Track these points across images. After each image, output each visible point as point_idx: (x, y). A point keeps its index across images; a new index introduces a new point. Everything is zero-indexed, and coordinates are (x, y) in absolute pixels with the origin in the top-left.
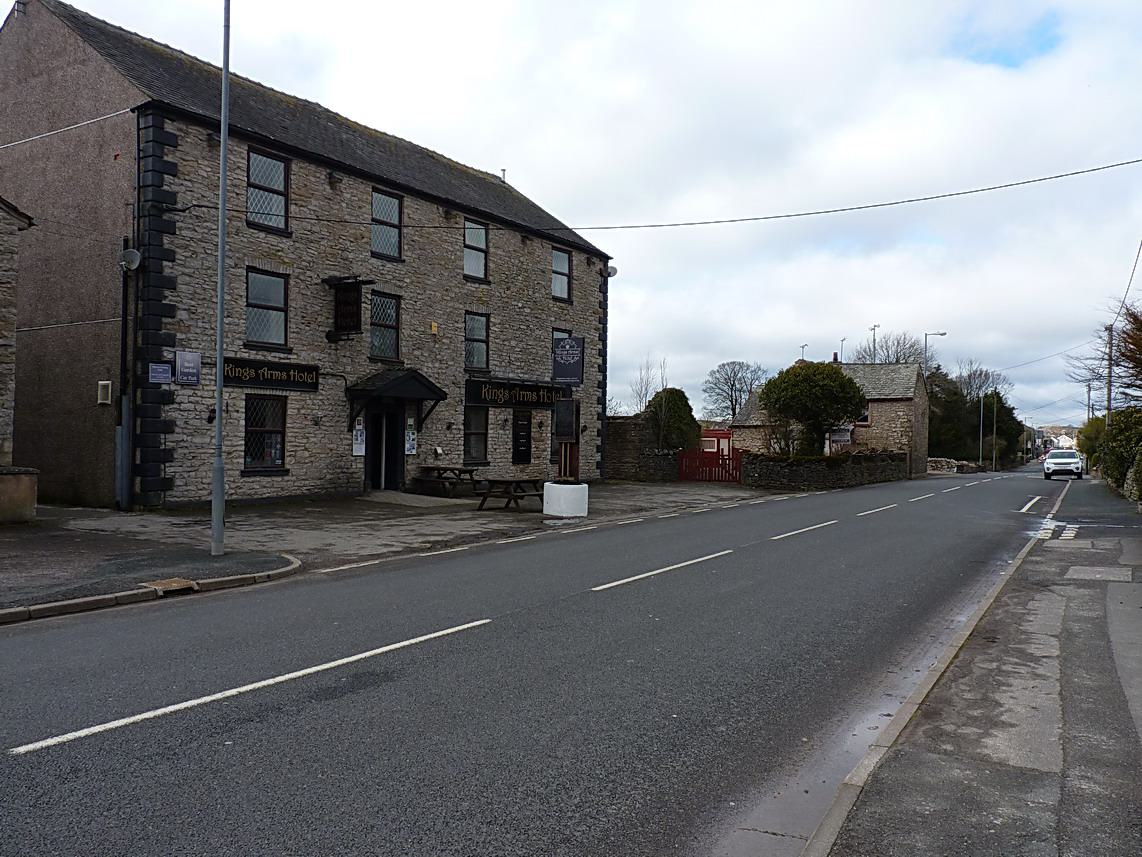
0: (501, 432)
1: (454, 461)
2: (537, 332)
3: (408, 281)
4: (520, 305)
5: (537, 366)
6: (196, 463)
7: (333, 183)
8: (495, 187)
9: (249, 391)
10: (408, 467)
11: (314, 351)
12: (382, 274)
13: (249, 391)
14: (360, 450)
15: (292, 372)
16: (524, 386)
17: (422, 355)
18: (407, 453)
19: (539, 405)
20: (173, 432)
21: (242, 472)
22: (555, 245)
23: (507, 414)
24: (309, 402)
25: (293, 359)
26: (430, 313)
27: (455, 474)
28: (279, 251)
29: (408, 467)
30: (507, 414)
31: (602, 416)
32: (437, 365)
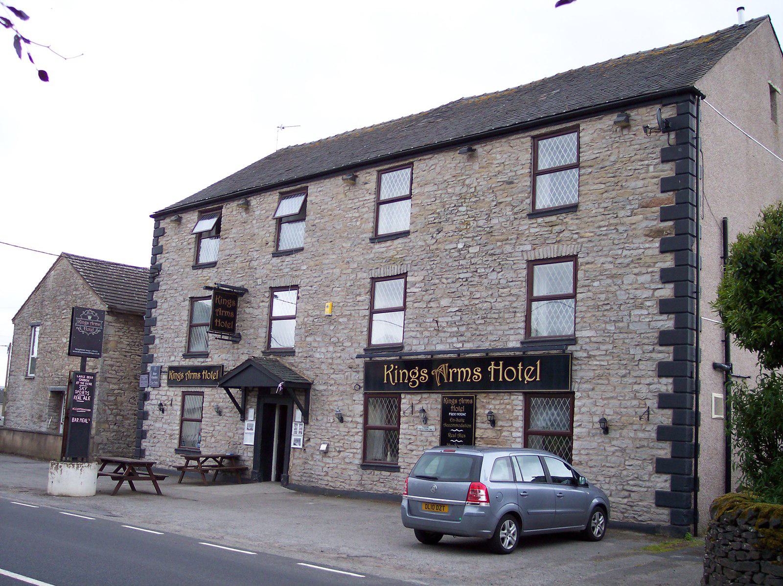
0: (420, 427)
1: (347, 460)
2: (493, 276)
3: (304, 267)
4: (460, 246)
5: (490, 328)
6: (156, 440)
7: (247, 207)
8: (760, 18)
9: (185, 389)
10: (295, 461)
11: (223, 353)
12: (281, 270)
13: (185, 389)
14: (249, 439)
15: (492, 367)
16: (460, 360)
17: (315, 340)
18: (292, 446)
19: (488, 385)
20: (147, 419)
21: (176, 450)
22: (282, 190)
23: (432, 403)
24: (217, 396)
25: (209, 362)
26: (326, 294)
27: (217, 461)
28: (207, 280)
29: (295, 461)
30: (432, 403)
31: (402, 393)
32: (331, 349)
